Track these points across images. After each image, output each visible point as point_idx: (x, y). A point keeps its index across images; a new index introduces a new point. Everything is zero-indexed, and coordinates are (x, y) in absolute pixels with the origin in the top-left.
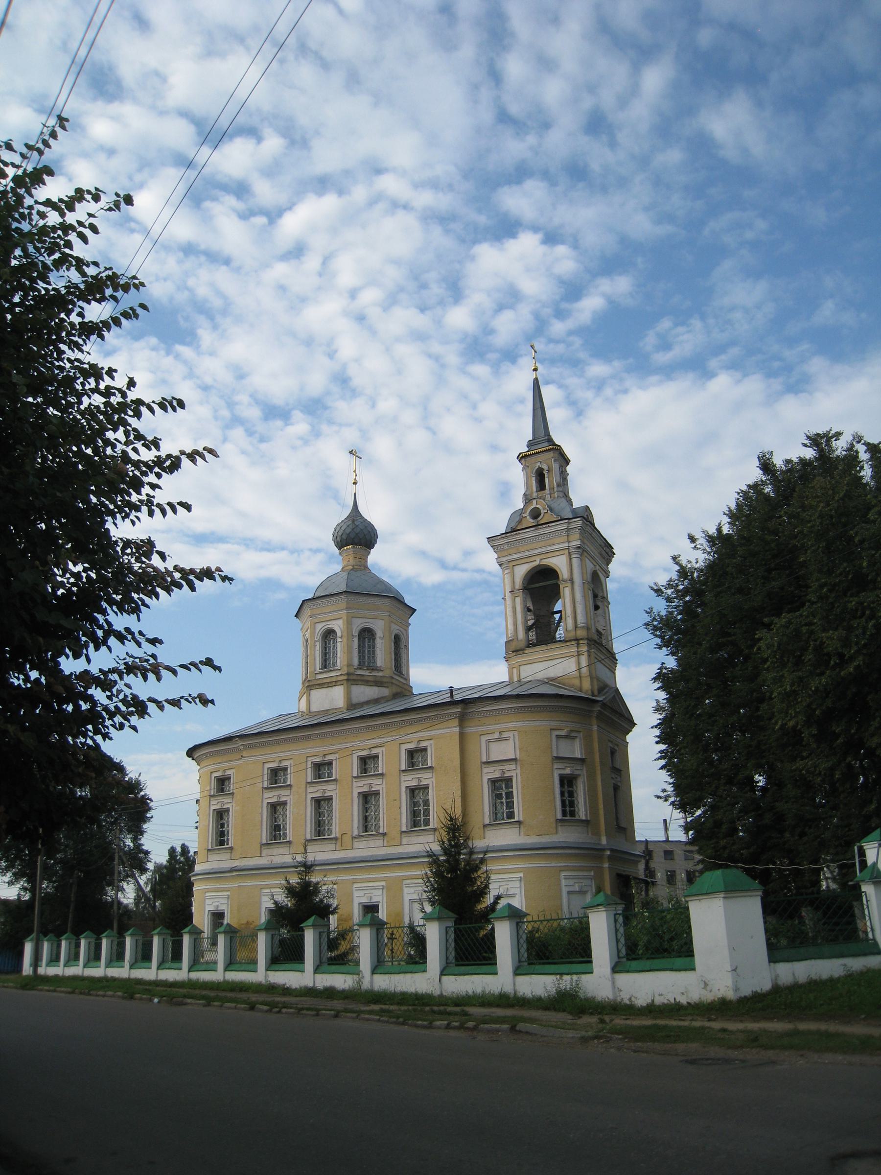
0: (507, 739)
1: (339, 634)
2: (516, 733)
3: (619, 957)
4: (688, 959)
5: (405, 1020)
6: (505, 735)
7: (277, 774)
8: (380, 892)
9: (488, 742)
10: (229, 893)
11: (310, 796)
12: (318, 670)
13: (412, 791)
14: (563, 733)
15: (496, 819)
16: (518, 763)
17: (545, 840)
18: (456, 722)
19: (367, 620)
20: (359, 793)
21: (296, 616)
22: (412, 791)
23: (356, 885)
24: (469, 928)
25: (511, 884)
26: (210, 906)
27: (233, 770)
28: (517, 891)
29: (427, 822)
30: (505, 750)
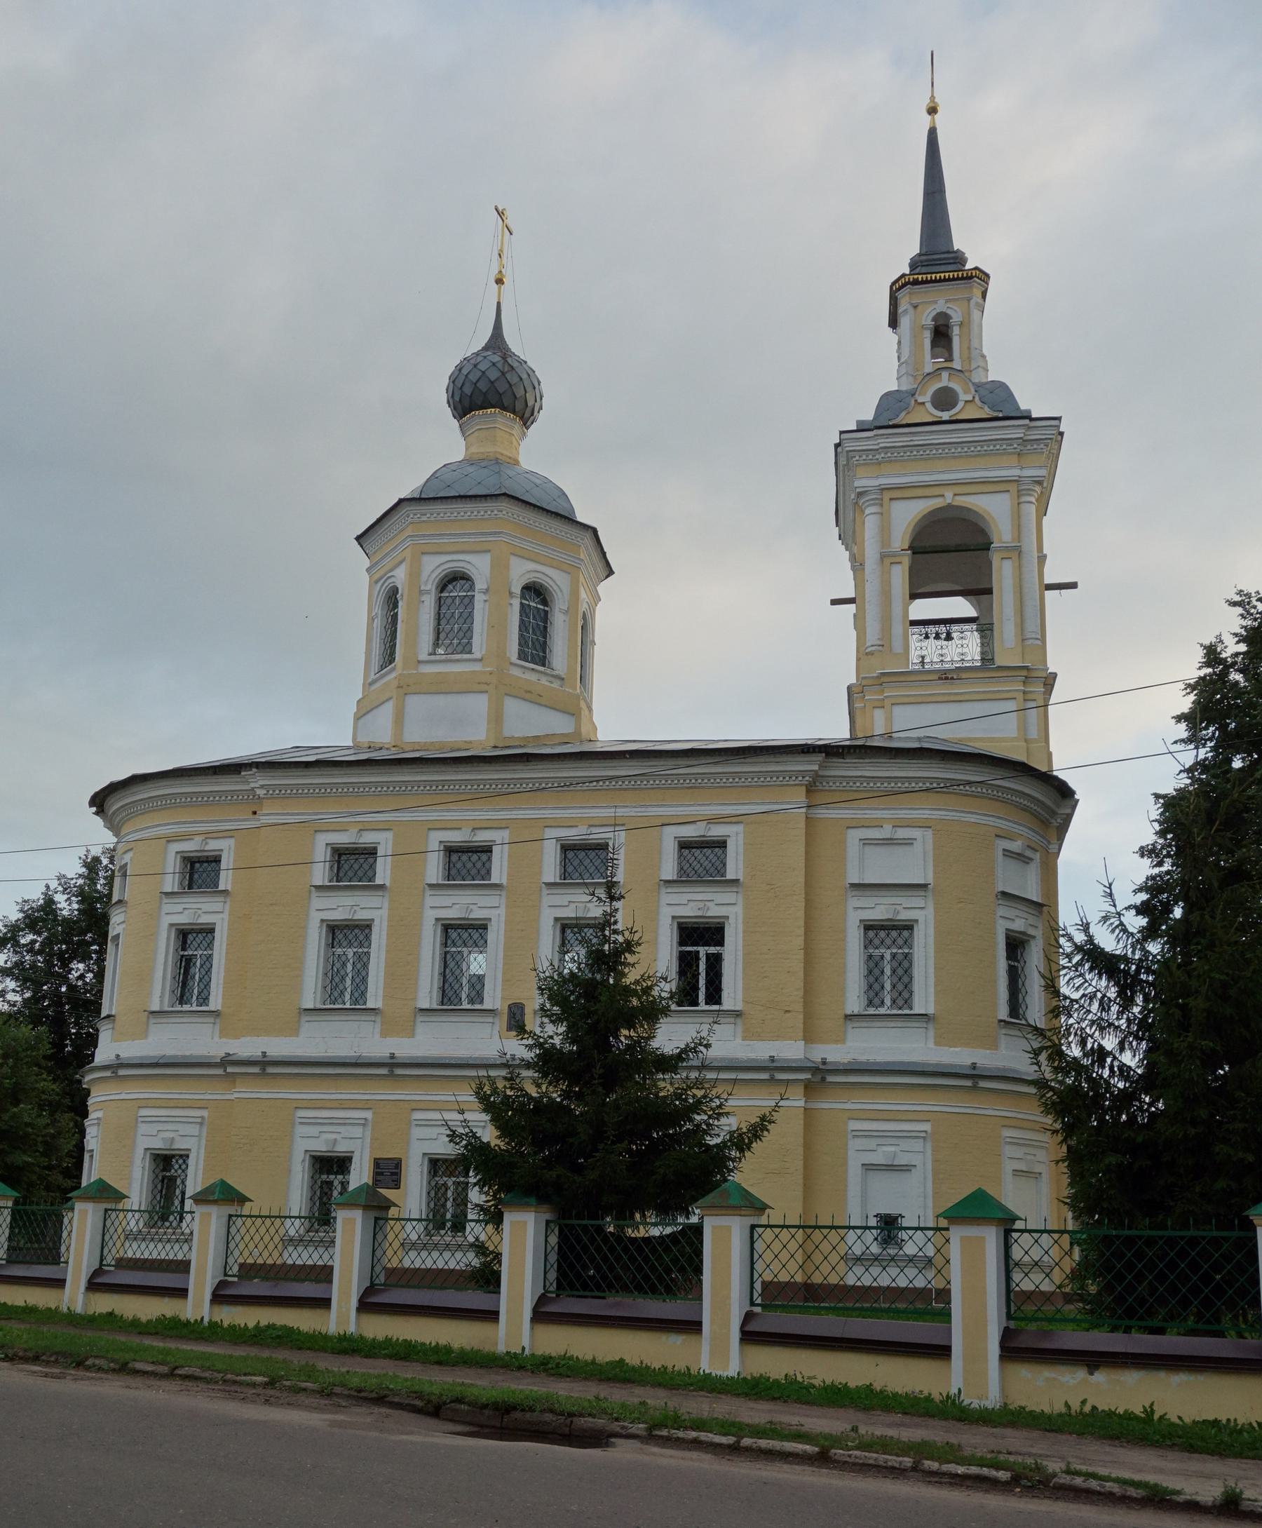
0: (908, 842)
1: (480, 585)
2: (929, 833)
3: (752, 1304)
4: (324, 1285)
5: (650, 1429)
6: (902, 833)
7: (352, 864)
8: (194, 1130)
9: (866, 842)
10: (205, 1113)
11: (166, 920)
12: (423, 656)
13: (184, 935)
14: (1016, 846)
15: (182, 1000)
16: (930, 894)
17: (959, 1056)
18: (800, 796)
19: (540, 568)
20: (172, 925)
21: (358, 538)
22: (184, 935)
23: (143, 1112)
24: (585, 1228)
25: (184, 1129)
26: (151, 1138)
27: (389, 835)
28: (915, 1160)
29: (204, 1000)
30: (912, 865)
